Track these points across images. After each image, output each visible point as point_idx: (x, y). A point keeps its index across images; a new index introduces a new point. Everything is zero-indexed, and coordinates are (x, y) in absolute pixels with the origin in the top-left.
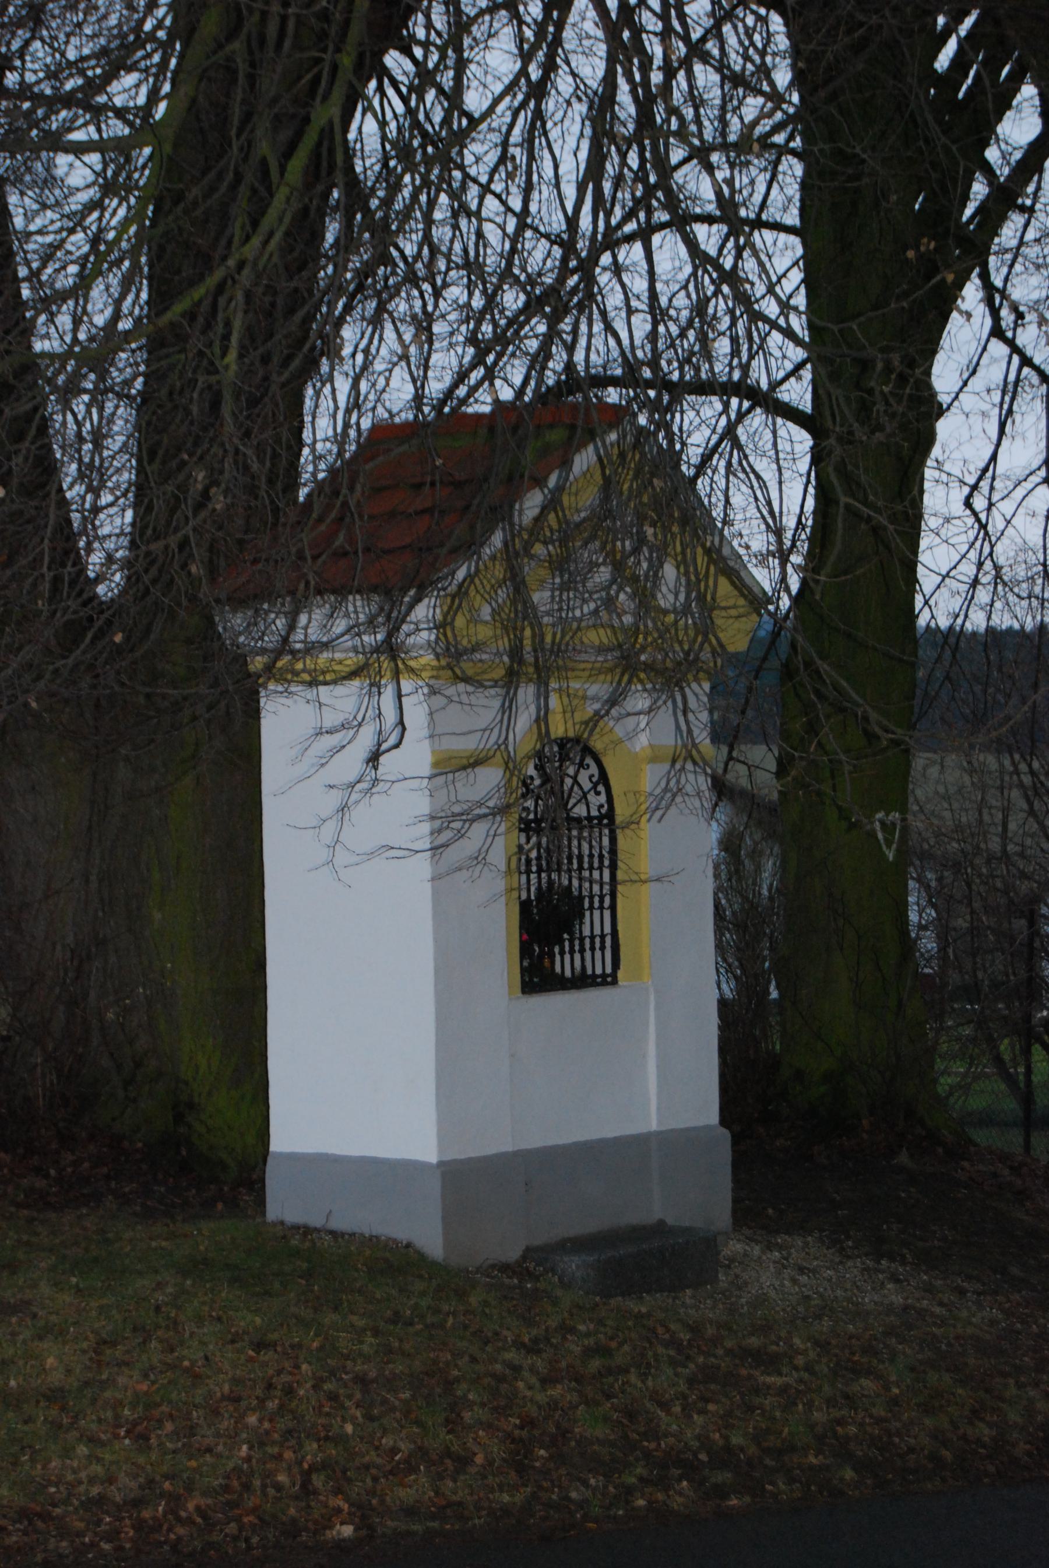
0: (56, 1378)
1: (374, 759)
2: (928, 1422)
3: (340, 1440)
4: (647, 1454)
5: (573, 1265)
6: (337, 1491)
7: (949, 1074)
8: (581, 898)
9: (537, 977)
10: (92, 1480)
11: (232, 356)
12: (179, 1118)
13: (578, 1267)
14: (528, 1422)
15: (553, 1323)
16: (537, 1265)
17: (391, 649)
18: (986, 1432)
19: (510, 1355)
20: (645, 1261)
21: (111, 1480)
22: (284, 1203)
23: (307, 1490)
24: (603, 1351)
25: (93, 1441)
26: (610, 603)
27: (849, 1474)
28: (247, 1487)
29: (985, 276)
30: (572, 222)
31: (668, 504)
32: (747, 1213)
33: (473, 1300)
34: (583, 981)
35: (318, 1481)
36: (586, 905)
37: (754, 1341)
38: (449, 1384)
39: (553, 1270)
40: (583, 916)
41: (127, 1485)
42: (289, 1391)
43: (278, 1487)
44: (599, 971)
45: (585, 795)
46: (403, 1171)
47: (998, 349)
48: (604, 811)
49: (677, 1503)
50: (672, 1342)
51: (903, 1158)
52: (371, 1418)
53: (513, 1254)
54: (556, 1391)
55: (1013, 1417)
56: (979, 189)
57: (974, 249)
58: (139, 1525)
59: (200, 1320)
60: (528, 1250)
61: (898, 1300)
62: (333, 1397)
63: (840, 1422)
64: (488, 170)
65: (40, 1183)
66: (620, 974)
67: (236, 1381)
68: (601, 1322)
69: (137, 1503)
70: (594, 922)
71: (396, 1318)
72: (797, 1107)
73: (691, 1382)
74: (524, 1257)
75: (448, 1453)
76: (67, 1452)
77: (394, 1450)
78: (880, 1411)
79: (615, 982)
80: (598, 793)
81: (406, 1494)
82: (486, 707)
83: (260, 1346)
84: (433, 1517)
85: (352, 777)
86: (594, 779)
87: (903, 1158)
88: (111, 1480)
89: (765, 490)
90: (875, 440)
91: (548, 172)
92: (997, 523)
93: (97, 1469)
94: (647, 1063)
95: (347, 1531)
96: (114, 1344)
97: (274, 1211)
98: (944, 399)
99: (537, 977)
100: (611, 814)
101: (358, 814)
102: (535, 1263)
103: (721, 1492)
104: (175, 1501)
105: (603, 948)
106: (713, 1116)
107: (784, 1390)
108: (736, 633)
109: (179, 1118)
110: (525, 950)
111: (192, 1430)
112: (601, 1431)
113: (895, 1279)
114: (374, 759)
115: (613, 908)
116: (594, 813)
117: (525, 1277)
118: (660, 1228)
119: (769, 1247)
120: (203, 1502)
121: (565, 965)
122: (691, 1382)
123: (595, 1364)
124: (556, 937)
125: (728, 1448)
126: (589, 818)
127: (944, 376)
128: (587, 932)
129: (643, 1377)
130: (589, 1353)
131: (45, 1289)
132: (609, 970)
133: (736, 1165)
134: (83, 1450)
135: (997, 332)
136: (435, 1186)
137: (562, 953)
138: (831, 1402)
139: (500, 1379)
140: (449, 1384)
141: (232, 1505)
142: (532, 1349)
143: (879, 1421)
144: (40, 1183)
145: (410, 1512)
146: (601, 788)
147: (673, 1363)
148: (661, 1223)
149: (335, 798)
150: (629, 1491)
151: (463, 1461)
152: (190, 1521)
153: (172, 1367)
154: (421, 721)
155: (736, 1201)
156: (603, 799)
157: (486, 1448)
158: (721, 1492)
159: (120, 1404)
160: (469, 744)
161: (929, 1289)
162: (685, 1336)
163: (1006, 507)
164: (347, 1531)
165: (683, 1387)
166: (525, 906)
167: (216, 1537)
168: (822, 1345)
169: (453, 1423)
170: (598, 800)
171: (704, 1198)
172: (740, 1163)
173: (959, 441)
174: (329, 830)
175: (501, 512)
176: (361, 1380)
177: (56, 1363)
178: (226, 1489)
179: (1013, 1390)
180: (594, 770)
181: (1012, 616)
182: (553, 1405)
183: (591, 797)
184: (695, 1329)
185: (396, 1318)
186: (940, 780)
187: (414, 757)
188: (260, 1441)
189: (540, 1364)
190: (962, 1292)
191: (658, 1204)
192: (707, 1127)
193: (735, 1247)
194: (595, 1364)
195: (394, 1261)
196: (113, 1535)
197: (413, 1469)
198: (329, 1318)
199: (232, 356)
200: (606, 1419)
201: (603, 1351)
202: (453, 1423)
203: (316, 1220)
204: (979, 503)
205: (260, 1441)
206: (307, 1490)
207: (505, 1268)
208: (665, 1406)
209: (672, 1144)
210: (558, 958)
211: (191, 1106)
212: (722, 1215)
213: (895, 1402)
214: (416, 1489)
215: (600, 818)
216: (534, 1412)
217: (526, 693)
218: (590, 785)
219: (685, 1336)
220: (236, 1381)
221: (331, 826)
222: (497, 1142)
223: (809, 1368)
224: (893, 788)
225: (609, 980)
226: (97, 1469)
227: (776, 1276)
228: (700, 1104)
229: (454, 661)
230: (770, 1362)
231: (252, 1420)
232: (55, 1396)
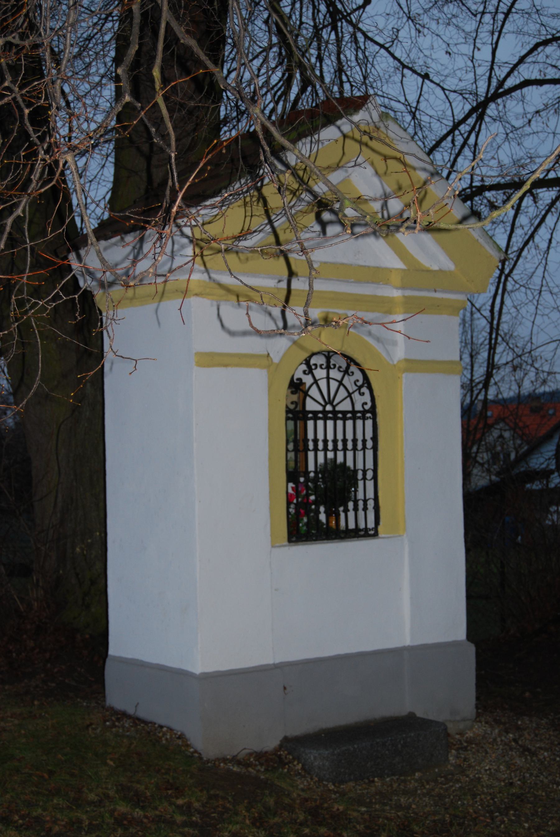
5: (315, 757)
8: (355, 471)
13: (315, 758)
16: (289, 754)
22: (117, 696)
34: (356, 533)
36: (360, 476)
39: (299, 759)
40: (356, 486)
44: (352, 526)
45: (350, 395)
48: (367, 407)
53: (271, 743)
60: (286, 740)
64: (527, 77)
66: (380, 528)
70: (364, 490)
74: (281, 746)
79: (376, 535)
80: (362, 394)
86: (359, 384)
105: (365, 509)
106: (460, 632)
115: (375, 478)
116: (358, 407)
124: (323, 501)
126: (354, 412)
128: (360, 495)
132: (371, 525)
137: (346, 511)
146: (365, 390)
148: (412, 716)
156: (367, 398)
171: (452, 698)
180: (358, 375)
183: (356, 396)
192: (462, 641)
210: (342, 515)
215: (364, 412)
218: (355, 388)
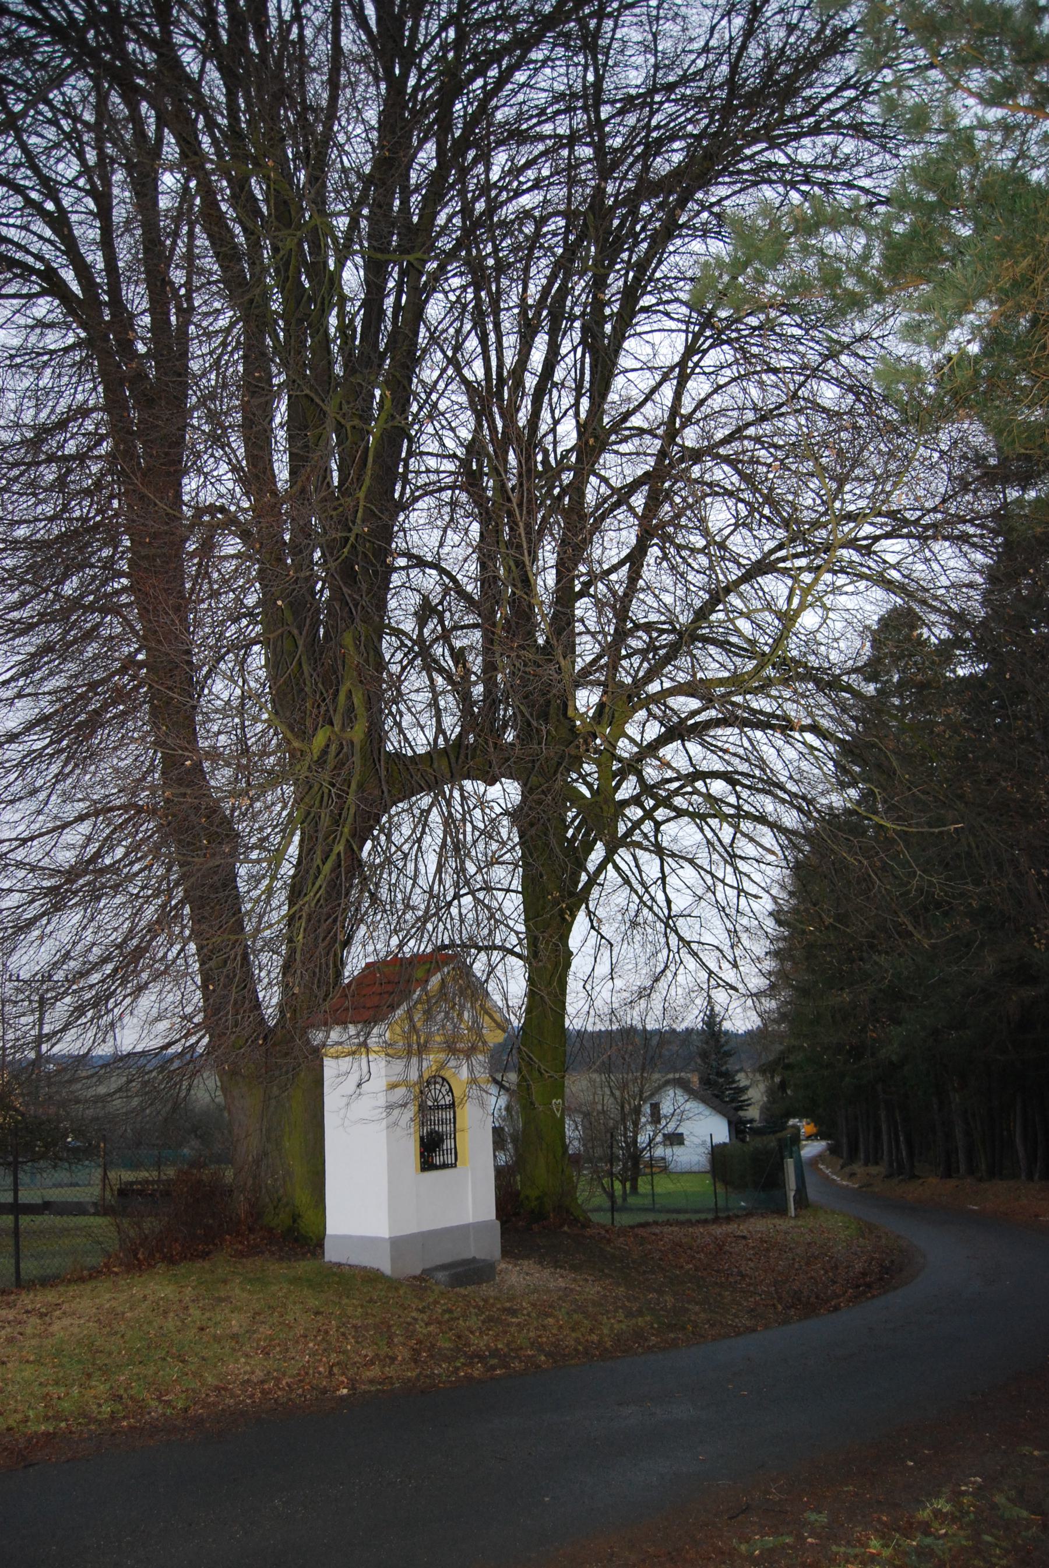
0: (235, 1330)
1: (359, 1085)
2: (574, 1335)
3: (345, 1352)
4: (465, 1353)
5: (441, 1276)
6: (343, 1374)
7: (581, 1196)
9: (427, 1165)
10: (245, 1373)
11: (301, 936)
12: (294, 1221)
14: (419, 1342)
15: (431, 1300)
17: (365, 1044)
18: (595, 1338)
19: (414, 1314)
20: (468, 1273)
21: (253, 1373)
22: (332, 1254)
23: (331, 1374)
24: (450, 1311)
25: (247, 1356)
26: (443, 1026)
27: (543, 1358)
28: (307, 1374)
29: (587, 908)
30: (431, 888)
31: (474, 991)
32: (507, 1252)
33: (401, 1292)
34: (444, 1166)
35: (335, 1370)
37: (508, 1305)
38: (389, 1327)
41: (259, 1374)
42: (327, 1332)
43: (320, 1373)
46: (374, 1241)
47: (593, 933)
49: (476, 1373)
50: (477, 1307)
51: (566, 1228)
52: (357, 1342)
53: (418, 1272)
54: (431, 1328)
55: (606, 1331)
56: (584, 877)
57: (583, 897)
58: (263, 1392)
59: (295, 1303)
61: (563, 1285)
62: (343, 1334)
63: (540, 1336)
65: (240, 1247)
67: (306, 1329)
68: (449, 1299)
69: (262, 1382)
70: (448, 1144)
71: (371, 1301)
72: (526, 1212)
73: (483, 1322)
75: (387, 1356)
76: (237, 1361)
77: (366, 1356)
78: (555, 1331)
81: (370, 1374)
82: (399, 1065)
83: (317, 1313)
84: (380, 1384)
85: (350, 1092)
87: (566, 1228)
88: (253, 1373)
89: (511, 984)
90: (549, 965)
91: (423, 871)
92: (594, 995)
93: (248, 1368)
94: (467, 1198)
95: (345, 1391)
96: (259, 1314)
97: (327, 1259)
98: (575, 951)
99: (427, 1165)
100: (453, 1104)
101: (353, 1106)
102: (427, 1274)
103: (493, 1368)
104: (278, 1380)
106: (494, 1217)
107: (519, 1324)
108: (494, 1037)
109: (294, 1221)
110: (422, 1155)
111: (287, 1350)
112: (447, 1345)
113: (562, 1276)
114: (359, 1085)
117: (421, 1282)
118: (474, 1260)
119: (516, 1265)
120: (289, 1380)
121: (438, 1161)
122: (483, 1322)
123: (447, 1316)
124: (433, 1151)
125: (497, 1349)
127: (574, 942)
129: (465, 1321)
130: (445, 1311)
131: (237, 1291)
133: (502, 1234)
134: (243, 1360)
135: (593, 927)
136: (387, 1247)
138: (537, 1329)
139: (409, 1324)
140: (389, 1327)
141: (300, 1381)
142: (422, 1311)
143: (555, 1335)
144: (240, 1247)
145: (371, 1382)
147: (477, 1315)
149: (345, 1100)
150: (457, 1369)
151: (393, 1359)
152: (283, 1389)
153: (280, 1323)
154: (381, 1071)
155: (503, 1247)
157: (402, 1353)
158: (493, 1368)
159: (260, 1340)
160: (394, 1079)
161: (575, 1280)
162: (481, 1304)
163: (598, 989)
164: (345, 1391)
165: (480, 1324)
166: (422, 1138)
167: (293, 1396)
168: (534, 1305)
169: (390, 1344)
170: (448, 1099)
171: (489, 1248)
172: (504, 1232)
173: (580, 966)
174: (343, 1111)
175: (407, 995)
176: (355, 1327)
177: (236, 1323)
178: (299, 1374)
179: (605, 1320)
181: (600, 1027)
182: (430, 1334)
184: (486, 1301)
185: (371, 1301)
186: (579, 1085)
187: (378, 1083)
188: (313, 1354)
189: (426, 1318)
190: (587, 1280)
191: (472, 1250)
193: (503, 1266)
194: (447, 1316)
195: (372, 1277)
196: (252, 1396)
197: (374, 1364)
198: (345, 1301)
199: (301, 936)
200: (450, 1339)
201: (450, 1311)
202: (390, 1344)
203: (344, 1261)
204: (588, 987)
205: (313, 1354)
206: (331, 1374)
207: (415, 1277)
208: (472, 1332)
209: (478, 1227)
211: (299, 1216)
212: (497, 1253)
213: (561, 1327)
214: (374, 1372)
216: (421, 1337)
217: (414, 1060)
219: (481, 1304)
220: (306, 1329)
221: (343, 1111)
222: (411, 1227)
223: (529, 1315)
224: (559, 1090)
225: (453, 1166)
226: (248, 1368)
227: (521, 1277)
228: (489, 1212)
229: (389, 1050)
230: (513, 1312)
231: (311, 1345)
232: (235, 1337)
